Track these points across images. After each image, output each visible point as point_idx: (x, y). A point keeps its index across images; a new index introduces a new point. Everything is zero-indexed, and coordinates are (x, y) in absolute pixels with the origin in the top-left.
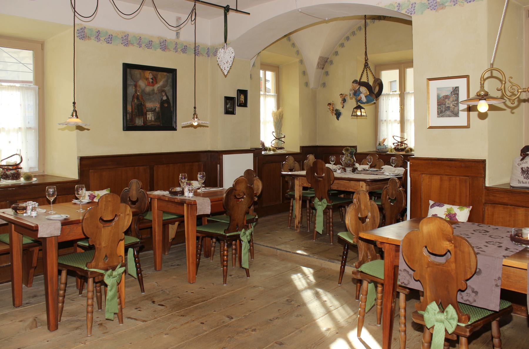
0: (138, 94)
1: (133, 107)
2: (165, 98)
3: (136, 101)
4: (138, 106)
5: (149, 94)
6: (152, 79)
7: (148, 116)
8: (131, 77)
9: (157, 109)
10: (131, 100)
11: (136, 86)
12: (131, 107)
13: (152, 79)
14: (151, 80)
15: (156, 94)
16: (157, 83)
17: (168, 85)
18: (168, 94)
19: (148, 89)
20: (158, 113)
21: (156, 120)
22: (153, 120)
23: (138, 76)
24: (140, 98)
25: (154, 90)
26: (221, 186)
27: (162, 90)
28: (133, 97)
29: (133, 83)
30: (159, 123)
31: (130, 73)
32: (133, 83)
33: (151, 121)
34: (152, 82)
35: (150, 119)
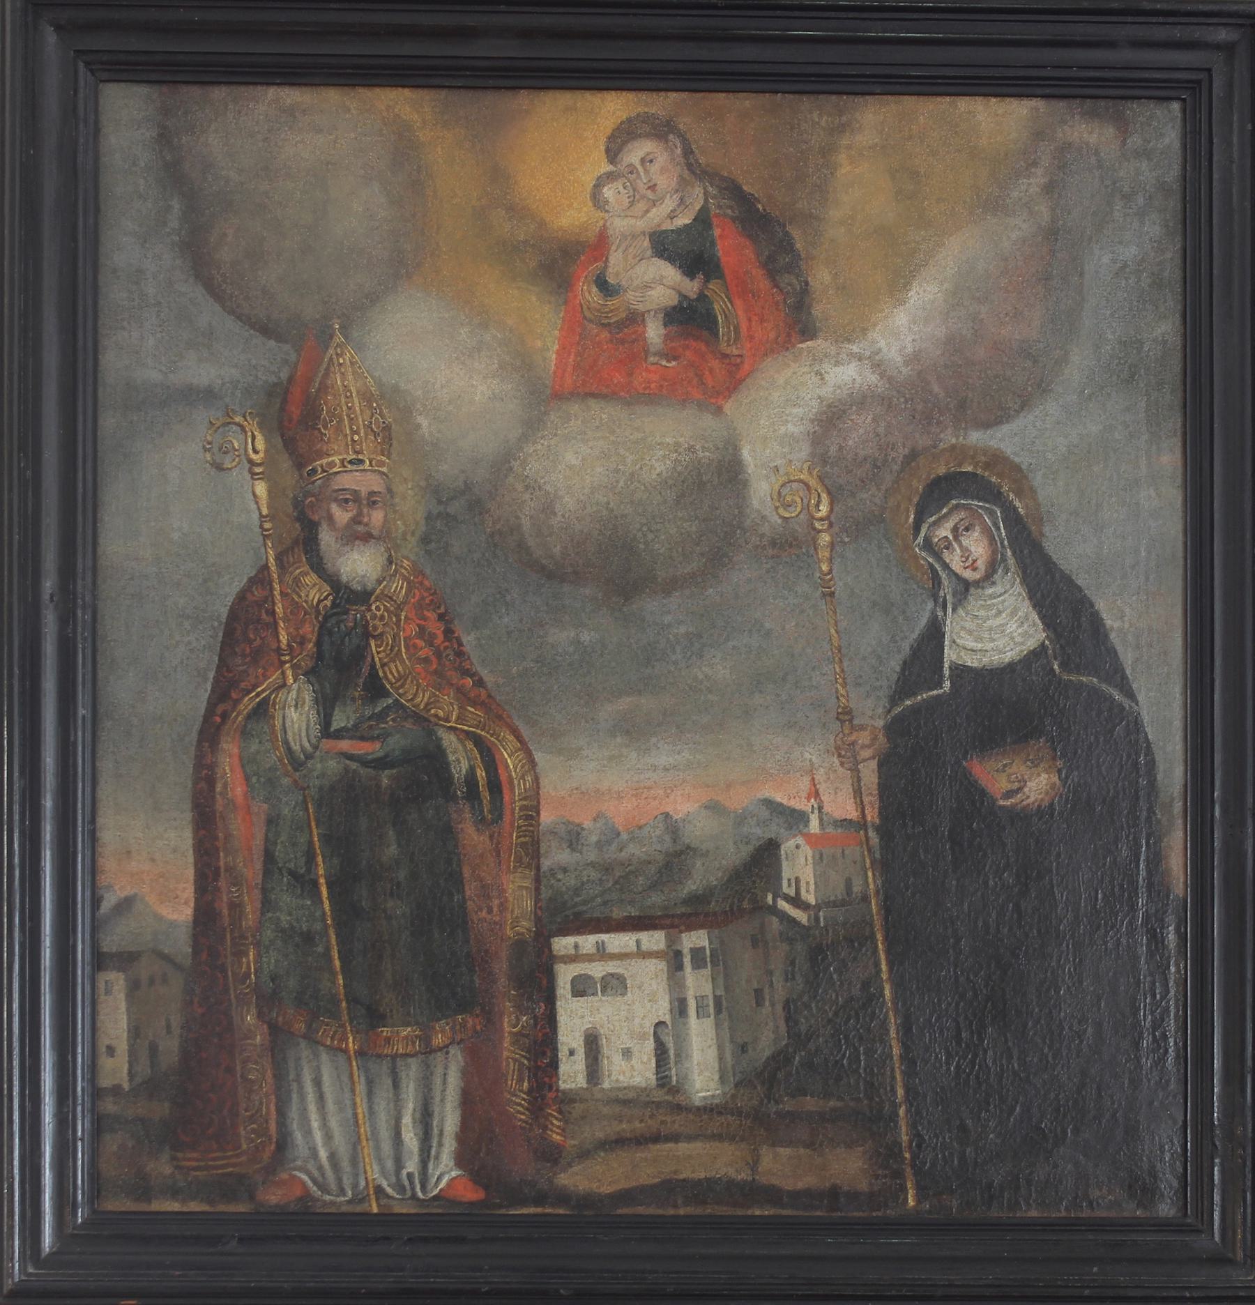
0: (359, 565)
1: (245, 833)
2: (996, 631)
3: (297, 715)
4: (345, 805)
5: (613, 567)
6: (689, 251)
7: (574, 1019)
8: (197, 254)
9: (800, 867)
10: (194, 699)
11: (296, 418)
12: (178, 838)
13: (689, 251)
14: (656, 284)
15: (789, 546)
16: (799, 323)
17: (1079, 364)
18: (1071, 550)
19: (593, 464)
20: (822, 950)
21: (766, 1095)
22: (703, 1077)
23: (359, 209)
24: (397, 659)
25: (730, 472)
26: (704, 948)
27: (933, 473)
28: (243, 632)
29: (233, 362)
30: (848, 1167)
31: (175, 174)
32: (233, 362)
33: (661, 1112)
34: (689, 318)
35: (631, 1070)
